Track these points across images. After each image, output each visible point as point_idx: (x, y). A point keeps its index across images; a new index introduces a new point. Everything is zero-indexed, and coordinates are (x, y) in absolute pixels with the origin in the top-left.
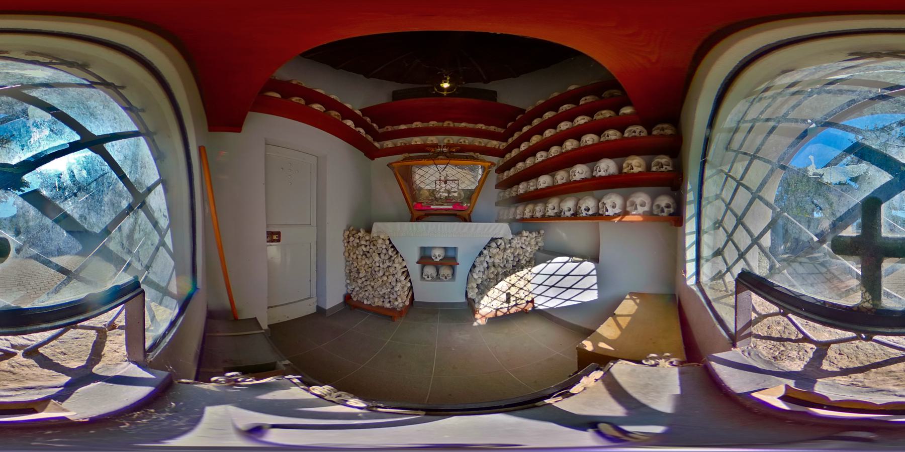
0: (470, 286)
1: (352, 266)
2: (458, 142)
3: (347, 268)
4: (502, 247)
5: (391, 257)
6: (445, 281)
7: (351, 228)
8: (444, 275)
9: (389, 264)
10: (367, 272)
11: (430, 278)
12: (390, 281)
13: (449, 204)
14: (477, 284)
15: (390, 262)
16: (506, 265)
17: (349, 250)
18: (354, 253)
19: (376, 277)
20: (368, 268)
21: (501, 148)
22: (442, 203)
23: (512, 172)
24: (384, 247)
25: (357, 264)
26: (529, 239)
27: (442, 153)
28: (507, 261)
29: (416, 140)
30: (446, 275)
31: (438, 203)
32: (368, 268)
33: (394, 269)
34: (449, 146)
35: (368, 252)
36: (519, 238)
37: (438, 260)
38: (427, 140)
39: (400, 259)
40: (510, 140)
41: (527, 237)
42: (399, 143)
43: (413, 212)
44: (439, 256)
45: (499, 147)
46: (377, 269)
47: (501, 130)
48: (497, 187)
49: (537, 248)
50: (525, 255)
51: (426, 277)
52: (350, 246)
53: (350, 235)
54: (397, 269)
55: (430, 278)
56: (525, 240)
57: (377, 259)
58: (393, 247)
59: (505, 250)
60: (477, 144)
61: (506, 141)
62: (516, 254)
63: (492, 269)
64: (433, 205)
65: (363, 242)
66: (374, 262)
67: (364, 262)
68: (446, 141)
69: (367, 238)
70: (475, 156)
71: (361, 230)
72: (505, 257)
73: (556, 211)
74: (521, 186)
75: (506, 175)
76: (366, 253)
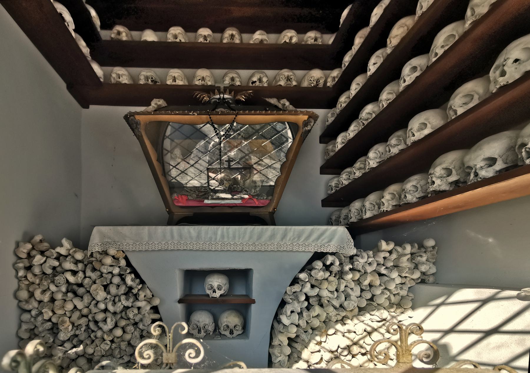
0: (276, 342)
1: (40, 319)
2: (248, 83)
3: (24, 327)
4: (336, 268)
5: (131, 288)
6: (229, 338)
7: (38, 238)
8: (228, 327)
9: (128, 304)
10: (78, 327)
11: (203, 334)
12: (128, 337)
14: (289, 339)
15: (127, 299)
16: (346, 304)
17: (28, 286)
18: (44, 292)
19: (99, 334)
20: (79, 318)
23: (353, 130)
24: (116, 271)
25: (51, 314)
26: (394, 256)
27: (222, 102)
28: (348, 296)
29: (176, 75)
30: (231, 326)
32: (79, 318)
33: (136, 311)
34: (232, 89)
35: (80, 285)
36: (371, 253)
37: (217, 294)
38: (194, 77)
40: (347, 59)
41: (390, 252)
42: (142, 77)
44: (219, 288)
45: (325, 82)
46: (100, 316)
47: (330, 39)
48: (324, 170)
49: (417, 275)
50: (386, 289)
52: (35, 275)
53: (34, 253)
54: (143, 312)
55: (203, 334)
56: (385, 258)
57: (101, 295)
58: (134, 271)
59: (341, 275)
60: (282, 83)
62: (366, 283)
63: (317, 310)
64: (208, 199)
65: (68, 265)
66: (94, 302)
67: (69, 306)
68: (227, 81)
69: (79, 256)
70: (280, 106)
71: (65, 242)
72: (342, 288)
73: (453, 178)
74: (371, 154)
76: (75, 287)
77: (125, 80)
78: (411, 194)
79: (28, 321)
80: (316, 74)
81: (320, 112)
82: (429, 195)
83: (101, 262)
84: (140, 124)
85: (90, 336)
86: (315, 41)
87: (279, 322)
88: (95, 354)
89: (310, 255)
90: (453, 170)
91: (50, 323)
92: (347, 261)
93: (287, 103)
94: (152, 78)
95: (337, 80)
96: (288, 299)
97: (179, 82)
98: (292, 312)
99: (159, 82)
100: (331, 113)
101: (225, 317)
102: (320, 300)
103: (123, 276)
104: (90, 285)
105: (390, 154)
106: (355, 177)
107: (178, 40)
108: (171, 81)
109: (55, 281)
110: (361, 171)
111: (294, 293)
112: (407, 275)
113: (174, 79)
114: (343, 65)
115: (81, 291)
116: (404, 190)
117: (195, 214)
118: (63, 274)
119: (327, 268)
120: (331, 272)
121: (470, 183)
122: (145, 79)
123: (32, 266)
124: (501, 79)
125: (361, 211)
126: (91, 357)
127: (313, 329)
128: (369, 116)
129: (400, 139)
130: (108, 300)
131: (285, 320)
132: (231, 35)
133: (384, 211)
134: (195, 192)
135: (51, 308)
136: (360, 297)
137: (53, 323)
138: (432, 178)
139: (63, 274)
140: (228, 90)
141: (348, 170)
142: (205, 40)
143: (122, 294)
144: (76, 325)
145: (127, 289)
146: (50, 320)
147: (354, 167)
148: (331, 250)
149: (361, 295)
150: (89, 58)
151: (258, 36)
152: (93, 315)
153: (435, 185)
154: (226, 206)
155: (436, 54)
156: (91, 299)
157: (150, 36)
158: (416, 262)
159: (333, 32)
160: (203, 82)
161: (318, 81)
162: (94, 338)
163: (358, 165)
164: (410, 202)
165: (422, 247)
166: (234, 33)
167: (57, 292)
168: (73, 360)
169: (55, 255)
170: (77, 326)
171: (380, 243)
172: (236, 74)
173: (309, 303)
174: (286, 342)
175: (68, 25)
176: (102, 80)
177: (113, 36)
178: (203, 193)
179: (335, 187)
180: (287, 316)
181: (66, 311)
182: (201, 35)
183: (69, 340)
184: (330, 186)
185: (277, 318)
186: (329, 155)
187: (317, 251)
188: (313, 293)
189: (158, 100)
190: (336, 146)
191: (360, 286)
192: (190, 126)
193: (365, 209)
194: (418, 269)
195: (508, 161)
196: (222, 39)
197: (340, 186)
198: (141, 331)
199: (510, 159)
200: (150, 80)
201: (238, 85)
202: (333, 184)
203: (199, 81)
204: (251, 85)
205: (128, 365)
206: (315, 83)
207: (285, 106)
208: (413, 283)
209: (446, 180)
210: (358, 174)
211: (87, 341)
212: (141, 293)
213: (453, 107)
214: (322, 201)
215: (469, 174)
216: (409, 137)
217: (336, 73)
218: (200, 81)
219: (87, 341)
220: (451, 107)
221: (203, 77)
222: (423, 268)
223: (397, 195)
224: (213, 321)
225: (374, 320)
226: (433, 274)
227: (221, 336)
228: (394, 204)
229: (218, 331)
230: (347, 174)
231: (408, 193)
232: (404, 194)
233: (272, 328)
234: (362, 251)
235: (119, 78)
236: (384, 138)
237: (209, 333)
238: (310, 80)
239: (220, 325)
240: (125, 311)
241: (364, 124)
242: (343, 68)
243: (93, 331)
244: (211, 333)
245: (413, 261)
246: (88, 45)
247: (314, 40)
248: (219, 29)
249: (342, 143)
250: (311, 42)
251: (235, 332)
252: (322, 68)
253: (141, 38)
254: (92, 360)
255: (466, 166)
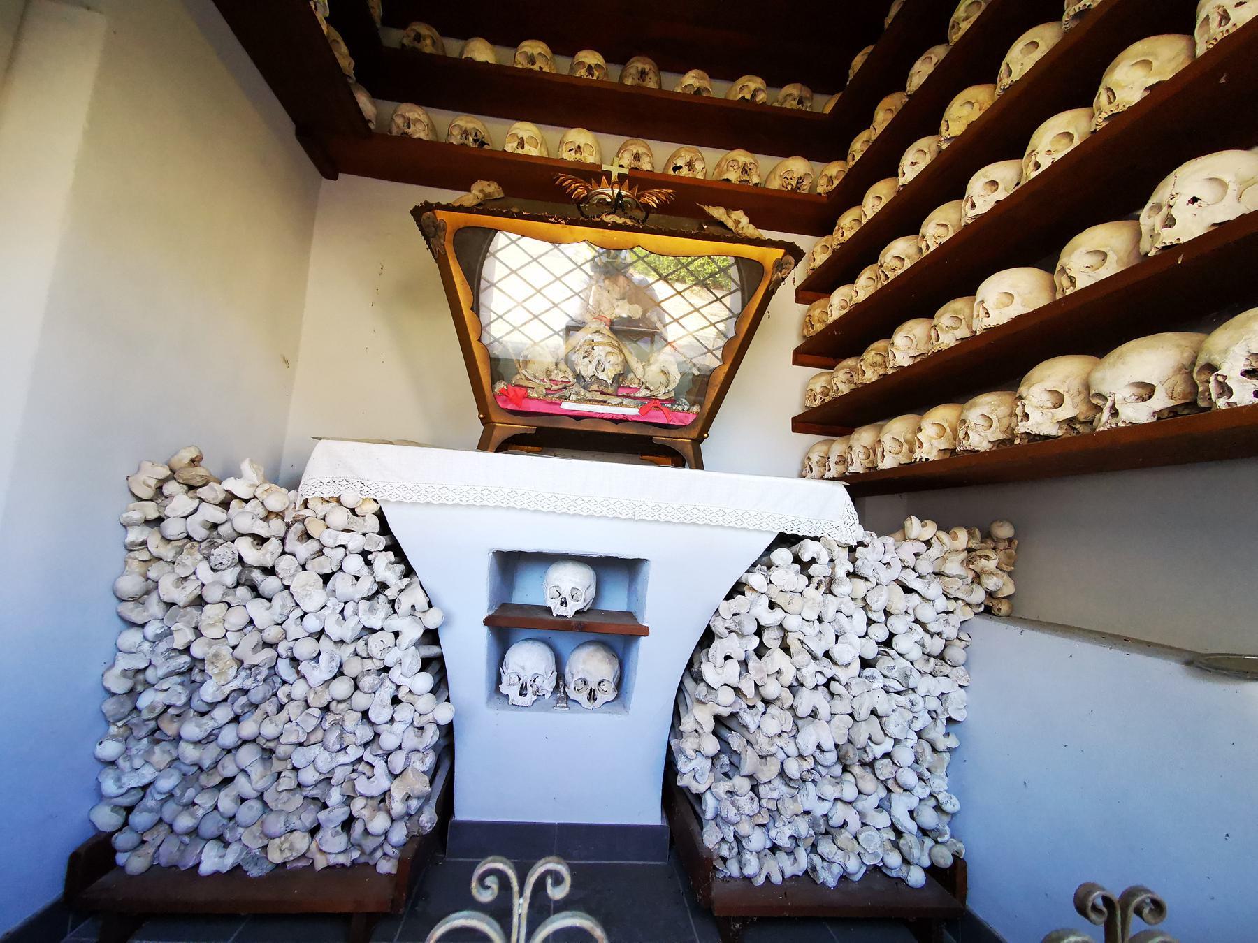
0: (687, 724)
1: (163, 646)
5: (383, 586)
11: (530, 697)
13: (625, 401)
14: (717, 718)
20: (255, 649)
21: (822, 189)
22: (602, 398)
23: (864, 287)
25: (190, 636)
31: (589, 396)
32: (255, 649)
34: (637, 180)
35: (270, 571)
39: (421, 601)
40: (858, 147)
42: (456, 132)
43: (495, 417)
46: (305, 649)
47: (826, 104)
48: (801, 357)
51: (513, 692)
58: (394, 547)
61: (842, 155)
63: (776, 658)
64: (567, 398)
65: (244, 518)
66: (298, 613)
67: (236, 618)
70: (731, 225)
71: (246, 467)
73: (1066, 412)
74: (899, 338)
75: (840, 302)
76: (257, 575)
77: (420, 132)
78: (977, 432)
79: (134, 650)
80: (797, 166)
81: (802, 241)
82: (1017, 442)
83: (324, 520)
84: (445, 229)
85: (276, 695)
86: (798, 104)
87: (699, 679)
88: (283, 740)
89: (770, 539)
90: (1066, 396)
91: (185, 659)
92: (843, 555)
93: (744, 220)
94: (476, 135)
95: (836, 183)
96: (718, 627)
97: (531, 151)
98: (727, 658)
99: (488, 145)
100: (820, 245)
101: (581, 660)
102: (784, 638)
103: (370, 557)
104: (292, 572)
105: (940, 344)
106: (864, 381)
107: (536, 67)
108: (515, 144)
109: (212, 558)
110: (876, 368)
111: (734, 615)
112: (960, 595)
113: (521, 143)
114: (850, 157)
115: (269, 584)
116: (964, 421)
117: (539, 429)
118: (233, 542)
119: (804, 566)
120: (810, 577)
121: (1101, 429)
122: (461, 136)
123: (163, 520)
124: (1166, 232)
125: (872, 451)
126: (271, 745)
127: (767, 702)
128: (897, 263)
129: (959, 317)
130: (330, 611)
131: (708, 671)
132: (642, 71)
133: (921, 458)
134: (543, 380)
135: (194, 621)
136: (864, 637)
137: (194, 659)
138: (1024, 406)
139: (233, 542)
140: (627, 181)
141: (850, 362)
142: (589, 75)
143: (363, 598)
144: (246, 665)
145: (376, 587)
146: (187, 650)
147: (862, 360)
148: (812, 531)
149: (867, 632)
150: (352, 80)
151: (692, 80)
152: (291, 644)
153: (1030, 422)
154: (606, 419)
155: (1037, 166)
156: (291, 604)
157: (481, 52)
158: (978, 570)
159: (831, 93)
160: (578, 155)
161: (800, 181)
162: (285, 700)
163: (871, 355)
164: (976, 449)
165: (987, 538)
166: (647, 68)
167: (214, 583)
168: (229, 751)
169: (221, 496)
170: (250, 669)
171: (909, 522)
172: (643, 147)
173: (761, 641)
174: (709, 725)
175: (316, 8)
176: (372, 126)
177: (405, 41)
178: (559, 386)
179: (822, 393)
180: (717, 665)
181: (227, 631)
182: (582, 63)
183: (225, 700)
184: (812, 390)
185: (692, 670)
186: (812, 328)
187: (786, 532)
188: (769, 618)
189: (486, 183)
190: (829, 313)
191: (866, 611)
192: (587, 277)
193: (881, 449)
194: (980, 584)
195: (1175, 394)
196: (621, 78)
197: (832, 394)
198: (394, 687)
199: (1179, 389)
200: (471, 139)
201: (645, 169)
202: (818, 389)
203: (571, 152)
204: (671, 172)
205: (355, 767)
206: (794, 183)
207: (740, 226)
208: (969, 614)
209: (1053, 414)
210: (871, 376)
211: (267, 707)
212: (403, 597)
213: (1067, 271)
214: (794, 420)
215: (1099, 409)
216: (978, 316)
217: (835, 169)
218: (573, 152)
219: (267, 707)
220: (1063, 269)
221: (579, 147)
222: (991, 583)
223: (948, 430)
224: (554, 668)
225: (891, 690)
226: (1008, 597)
227: (570, 703)
228: (943, 447)
229: (562, 690)
230: (848, 370)
231: (972, 430)
232: (965, 430)
233: (681, 689)
234: (874, 534)
235: (409, 127)
236: (928, 311)
237: (544, 695)
238: (786, 177)
239: (568, 677)
240: (365, 637)
241: (887, 276)
242: (852, 163)
243: (284, 682)
244: (548, 695)
245: (971, 566)
246: (353, 54)
247: (796, 102)
248: (617, 56)
249: (842, 307)
250: (791, 104)
251: (599, 695)
252: (810, 157)
253: (462, 53)
254: (274, 753)
255: (1093, 392)
